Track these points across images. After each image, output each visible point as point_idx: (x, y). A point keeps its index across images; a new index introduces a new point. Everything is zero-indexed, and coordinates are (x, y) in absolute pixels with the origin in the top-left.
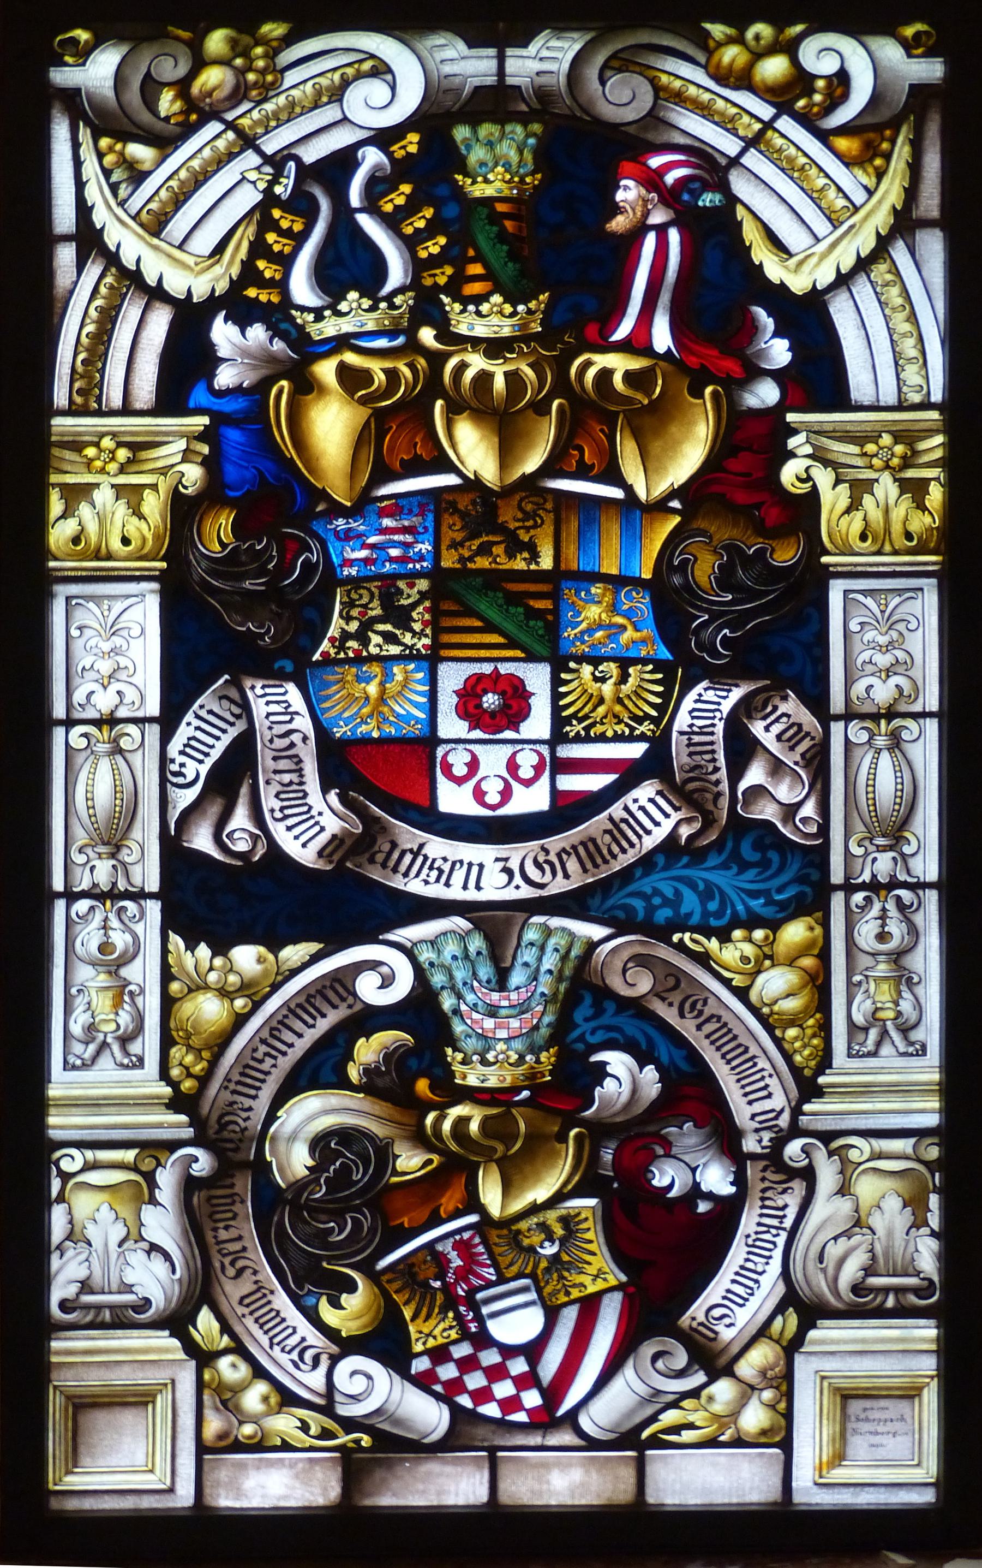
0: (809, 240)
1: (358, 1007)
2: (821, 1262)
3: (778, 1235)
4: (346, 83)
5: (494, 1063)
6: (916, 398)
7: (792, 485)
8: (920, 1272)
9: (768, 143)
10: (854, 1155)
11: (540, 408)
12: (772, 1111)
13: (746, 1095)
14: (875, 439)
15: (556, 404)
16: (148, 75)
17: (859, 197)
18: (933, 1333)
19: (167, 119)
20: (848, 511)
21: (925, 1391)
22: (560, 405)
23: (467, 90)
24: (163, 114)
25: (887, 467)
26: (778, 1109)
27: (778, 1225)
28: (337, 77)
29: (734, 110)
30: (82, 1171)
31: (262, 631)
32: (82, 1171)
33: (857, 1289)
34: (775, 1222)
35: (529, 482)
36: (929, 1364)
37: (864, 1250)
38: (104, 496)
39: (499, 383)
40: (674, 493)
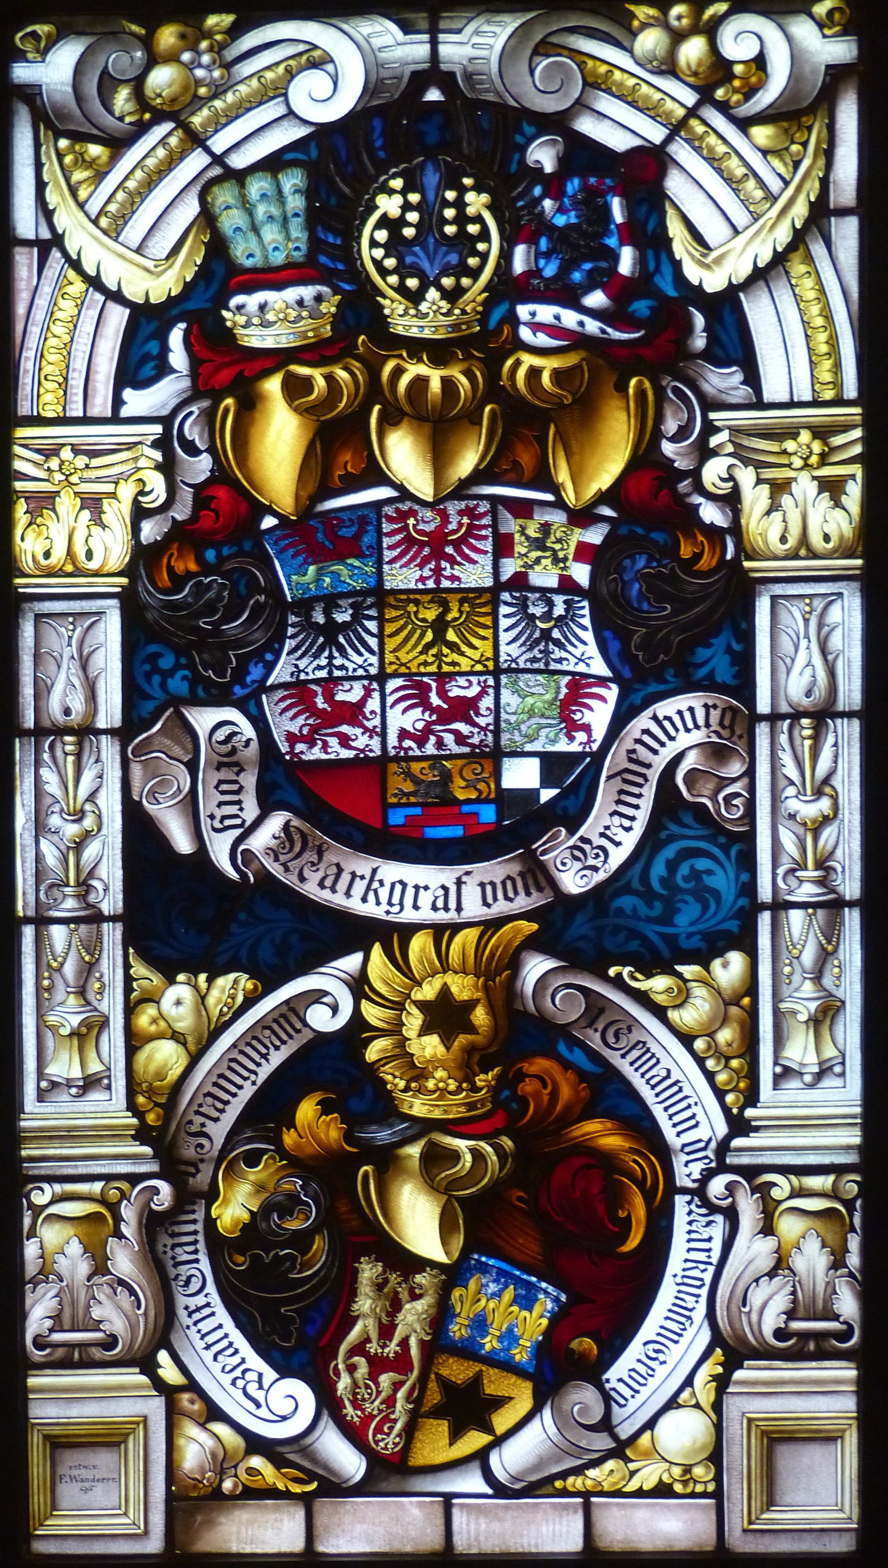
0: (727, 231)
1: (310, 1035)
2: (744, 1305)
3: (705, 1270)
4: (291, 75)
5: (435, 1092)
6: (828, 395)
7: (713, 484)
8: (839, 1316)
9: (690, 130)
10: (776, 1193)
11: (472, 417)
12: (700, 1141)
13: (675, 1125)
14: (795, 436)
15: (488, 409)
16: (105, 72)
17: (775, 185)
18: (853, 1373)
19: (121, 119)
20: (768, 513)
21: (847, 1434)
22: (492, 410)
23: (406, 79)
24: (117, 114)
25: (806, 466)
26: (706, 1139)
27: (706, 1260)
28: (281, 69)
29: (658, 96)
30: (52, 1202)
31: (130, 749)
32: (52, 1202)
33: (780, 1334)
34: (702, 1256)
35: (461, 490)
36: (849, 1404)
37: (788, 1292)
38: (66, 503)
39: (435, 385)
40: (603, 498)
